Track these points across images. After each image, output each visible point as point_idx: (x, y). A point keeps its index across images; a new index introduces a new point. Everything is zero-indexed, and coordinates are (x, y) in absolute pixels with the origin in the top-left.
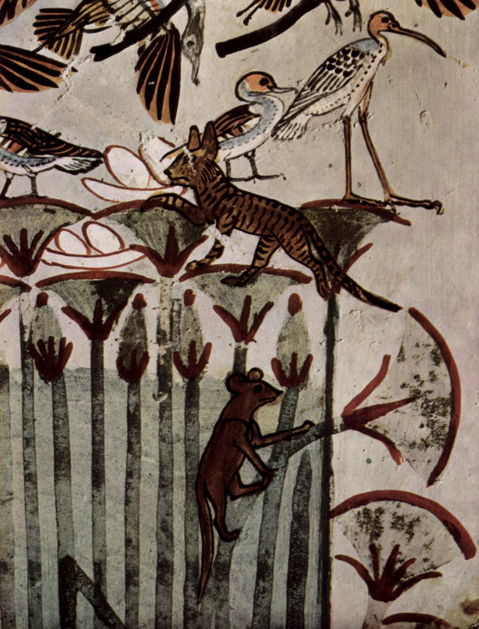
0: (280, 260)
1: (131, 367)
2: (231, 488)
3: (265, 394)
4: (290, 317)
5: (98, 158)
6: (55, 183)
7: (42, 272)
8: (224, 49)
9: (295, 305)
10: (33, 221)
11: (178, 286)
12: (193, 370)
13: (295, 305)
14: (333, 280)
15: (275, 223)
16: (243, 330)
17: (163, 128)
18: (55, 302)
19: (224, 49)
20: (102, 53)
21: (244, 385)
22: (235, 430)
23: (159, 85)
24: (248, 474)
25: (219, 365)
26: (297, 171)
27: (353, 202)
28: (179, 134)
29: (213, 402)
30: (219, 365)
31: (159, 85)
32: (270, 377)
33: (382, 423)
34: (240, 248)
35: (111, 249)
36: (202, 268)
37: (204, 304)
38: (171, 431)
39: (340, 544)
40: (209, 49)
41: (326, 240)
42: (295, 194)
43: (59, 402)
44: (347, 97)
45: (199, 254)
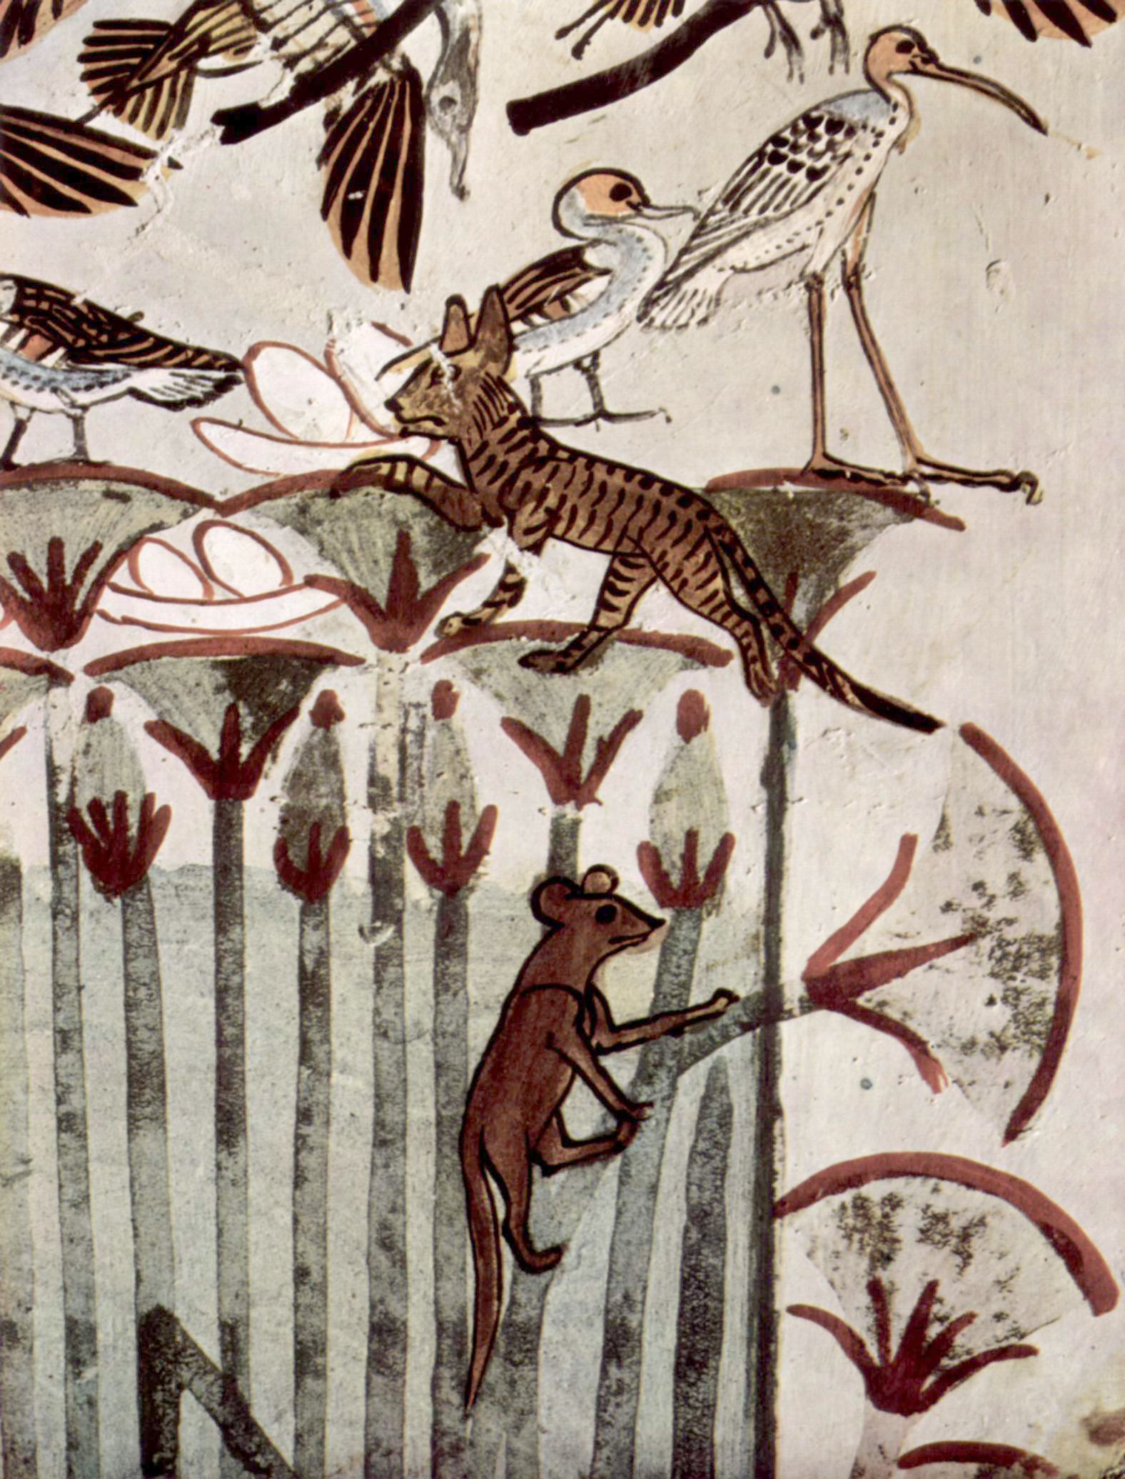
0: (658, 611)
1: (308, 872)
2: (541, 1147)
3: (620, 924)
4: (681, 745)
5: (229, 372)
6: (130, 426)
7: (99, 639)
8: (527, 115)
9: (692, 718)
10: (79, 519)
11: (416, 671)
12: (453, 873)
13: (692, 718)
14: (782, 652)
15: (652, 524)
16: (571, 776)
17: (384, 299)
18: (130, 710)
19: (527, 115)
20: (240, 123)
21: (571, 903)
22: (552, 1015)
23: (375, 196)
24: (583, 1115)
25: (513, 863)
26: (697, 401)
27: (830, 474)
28: (420, 314)
29: (502, 940)
30: (513, 863)
31: (375, 196)
32: (634, 887)
33: (895, 995)
34: (564, 583)
35: (262, 587)
36: (473, 630)
37: (478, 714)
38: (411, 1010)
39: (797, 1280)
40: (491, 116)
41: (762, 566)
42: (691, 458)
43: (139, 944)
44: (813, 229)
45: (467, 596)
